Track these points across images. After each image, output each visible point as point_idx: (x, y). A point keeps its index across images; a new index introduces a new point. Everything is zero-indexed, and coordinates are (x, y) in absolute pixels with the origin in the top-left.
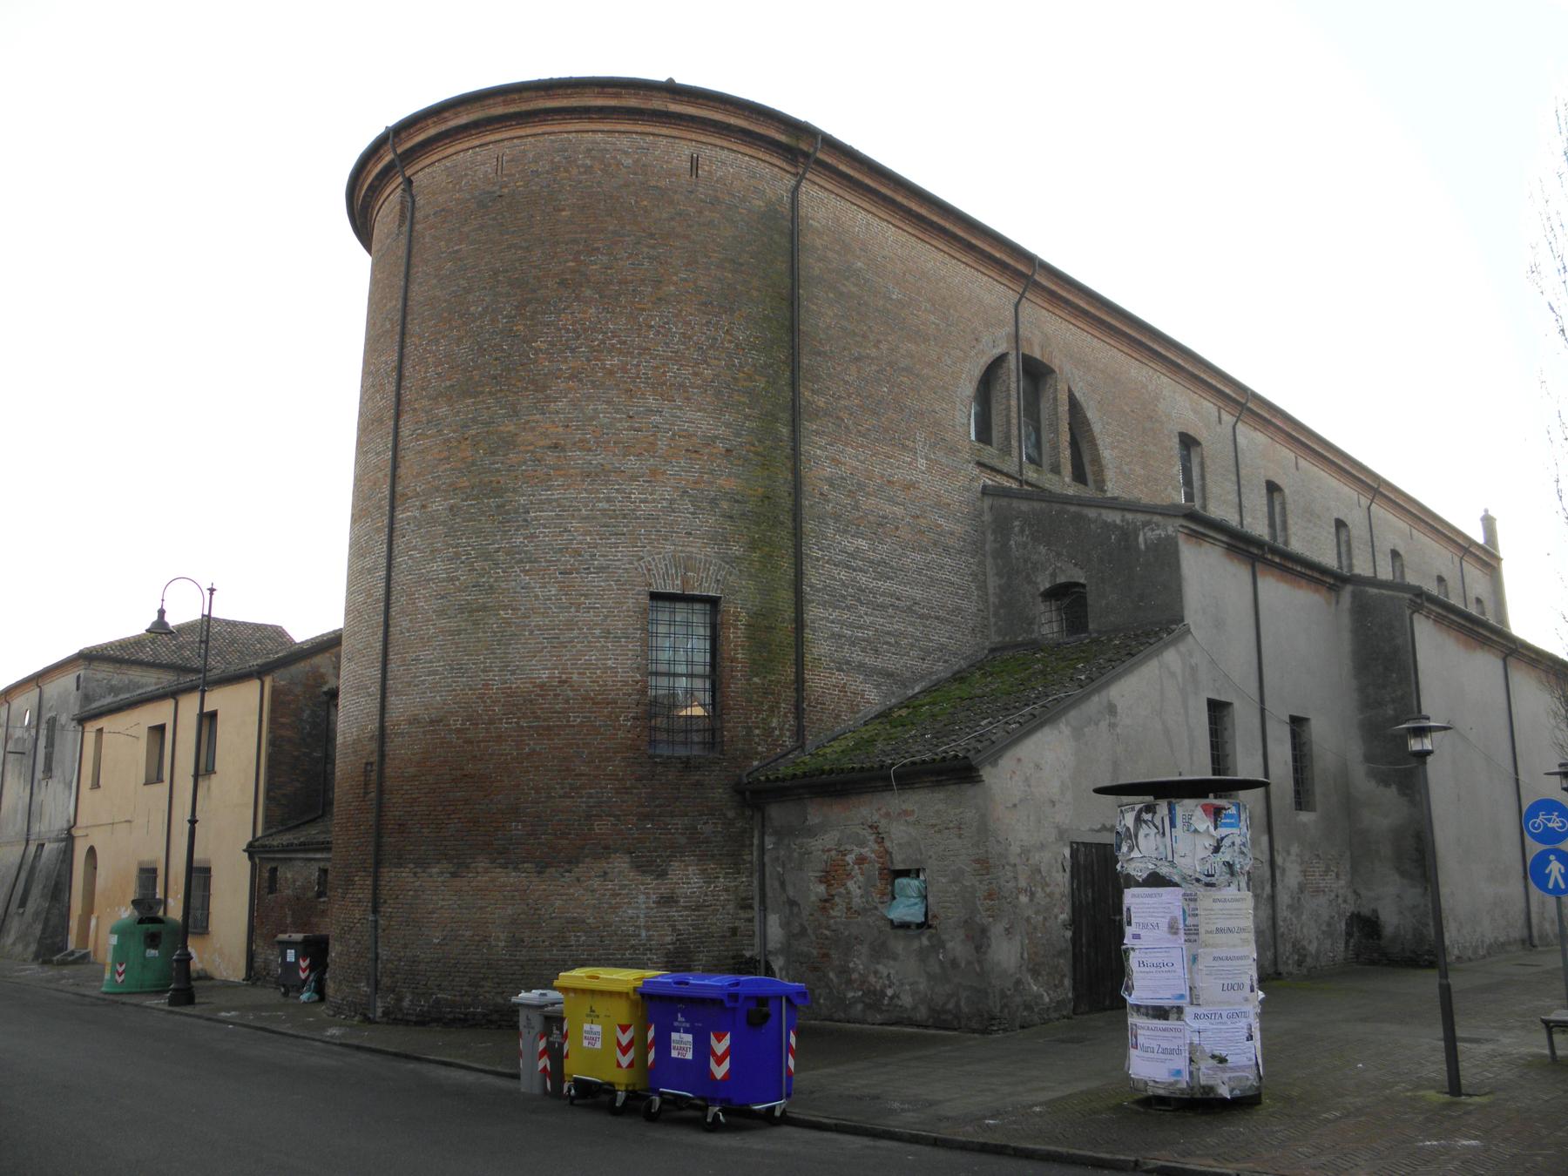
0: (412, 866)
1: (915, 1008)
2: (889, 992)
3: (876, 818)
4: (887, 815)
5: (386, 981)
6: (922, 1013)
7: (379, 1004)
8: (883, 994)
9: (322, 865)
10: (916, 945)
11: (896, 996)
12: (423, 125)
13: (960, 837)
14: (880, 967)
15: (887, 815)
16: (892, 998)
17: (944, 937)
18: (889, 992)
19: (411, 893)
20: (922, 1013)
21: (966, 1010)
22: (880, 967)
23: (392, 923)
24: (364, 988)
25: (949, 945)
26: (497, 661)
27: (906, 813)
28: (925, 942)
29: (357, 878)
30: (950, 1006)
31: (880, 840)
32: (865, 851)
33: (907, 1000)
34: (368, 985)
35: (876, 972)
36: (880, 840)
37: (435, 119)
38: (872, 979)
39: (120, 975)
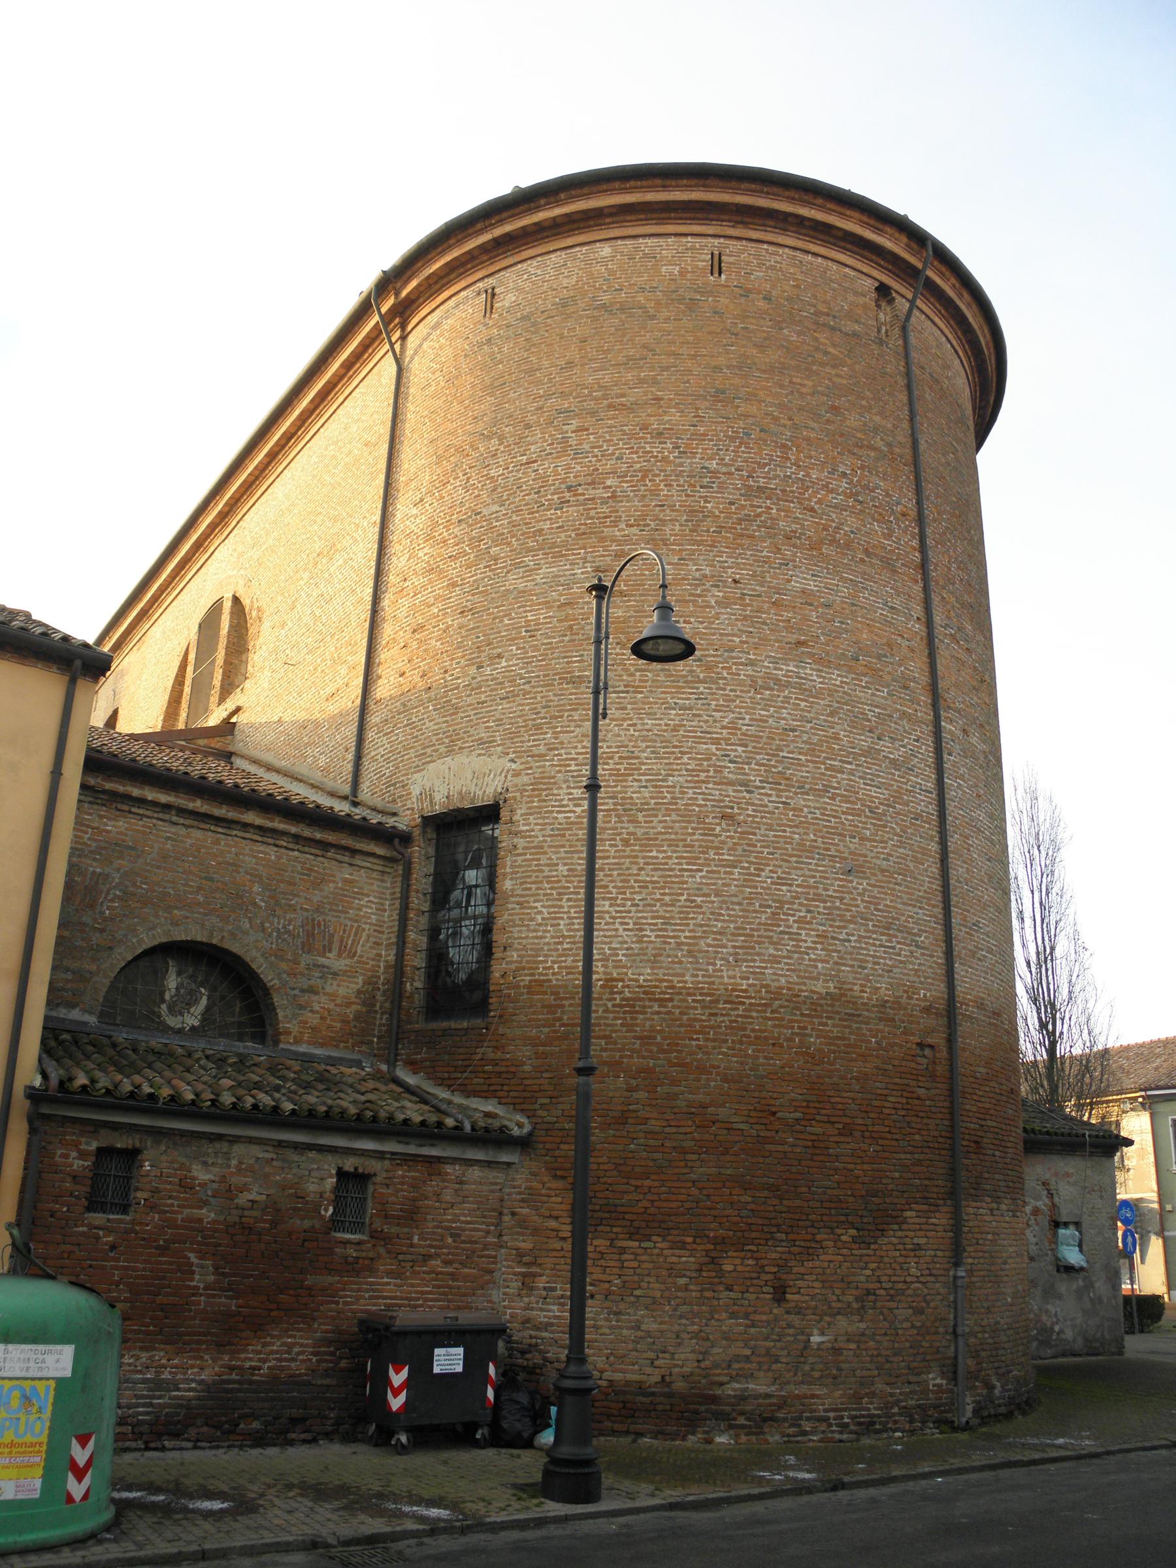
0: (988, 1199)
1: (1074, 1340)
2: (1057, 1328)
3: (1047, 1176)
4: (1056, 1174)
5: (967, 1363)
6: (1079, 1344)
7: (968, 1400)
8: (1052, 1329)
9: (349, 1164)
10: (1074, 1287)
11: (1061, 1332)
12: (948, 274)
13: (1101, 1197)
14: (1049, 1307)
15: (1056, 1174)
16: (1058, 1333)
17: (1094, 1279)
18: (1057, 1328)
19: (990, 1237)
20: (1079, 1344)
21: (1107, 1337)
22: (1049, 1307)
23: (974, 1279)
24: (934, 1379)
25: (1097, 1285)
26: (899, 934)
27: (1067, 1175)
28: (1081, 1283)
29: (908, 1214)
30: (1099, 1335)
31: (1051, 1195)
32: (1039, 1204)
33: (1069, 1334)
34: (943, 1375)
35: (1047, 1311)
36: (1051, 1195)
37: (957, 285)
38: (1044, 1318)
39: (80, 1474)
